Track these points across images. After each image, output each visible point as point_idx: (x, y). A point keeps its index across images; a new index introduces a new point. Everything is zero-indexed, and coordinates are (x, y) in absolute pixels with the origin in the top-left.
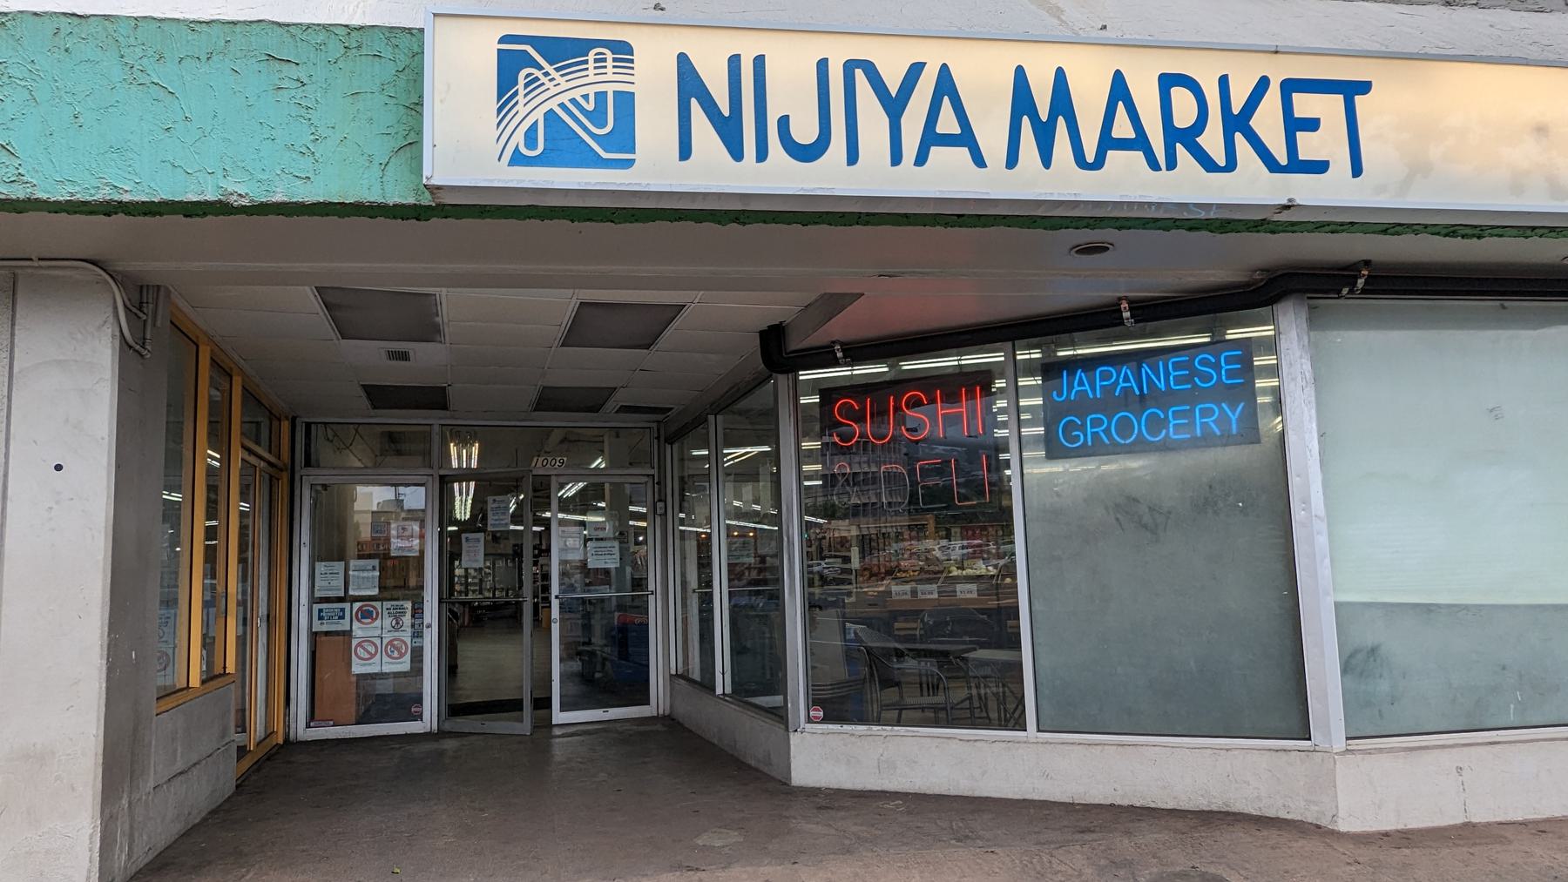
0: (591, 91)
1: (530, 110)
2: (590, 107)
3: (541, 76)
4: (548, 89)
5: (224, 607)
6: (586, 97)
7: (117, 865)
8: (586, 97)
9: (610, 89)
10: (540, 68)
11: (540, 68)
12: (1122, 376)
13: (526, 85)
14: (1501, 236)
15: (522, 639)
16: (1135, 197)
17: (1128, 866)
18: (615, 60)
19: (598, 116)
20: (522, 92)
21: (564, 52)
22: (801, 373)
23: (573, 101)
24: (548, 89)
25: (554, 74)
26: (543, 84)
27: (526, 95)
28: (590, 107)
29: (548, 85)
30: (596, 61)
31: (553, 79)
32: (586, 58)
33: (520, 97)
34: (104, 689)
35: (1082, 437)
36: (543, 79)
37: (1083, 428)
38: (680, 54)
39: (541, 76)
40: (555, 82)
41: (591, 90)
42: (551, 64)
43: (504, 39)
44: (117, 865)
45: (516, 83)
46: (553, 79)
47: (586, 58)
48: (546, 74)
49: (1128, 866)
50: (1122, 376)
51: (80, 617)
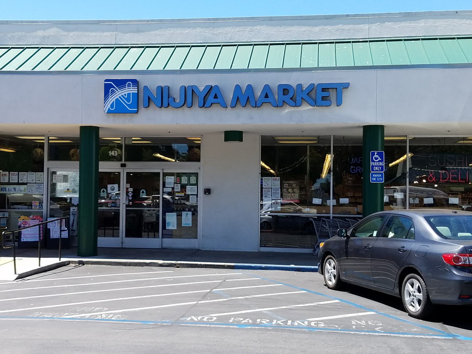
1: (112, 99)
3: (115, 90)
4: (117, 93)
6: (125, 95)
7: (301, 159)
9: (131, 92)
11: (115, 88)
12: (355, 160)
13: (111, 93)
14: (24, 198)
18: (132, 85)
19: (128, 100)
20: (110, 95)
24: (117, 93)
25: (118, 89)
26: (115, 92)
27: (111, 95)
29: (117, 92)
30: (128, 85)
31: (118, 90)
32: (119, 98)
33: (110, 96)
35: (355, 171)
37: (356, 169)
39: (115, 90)
40: (118, 91)
41: (126, 93)
42: (117, 87)
43: (106, 80)
44: (301, 159)
45: (109, 92)
47: (119, 98)
48: (116, 89)
50: (355, 160)
51: (24, 122)
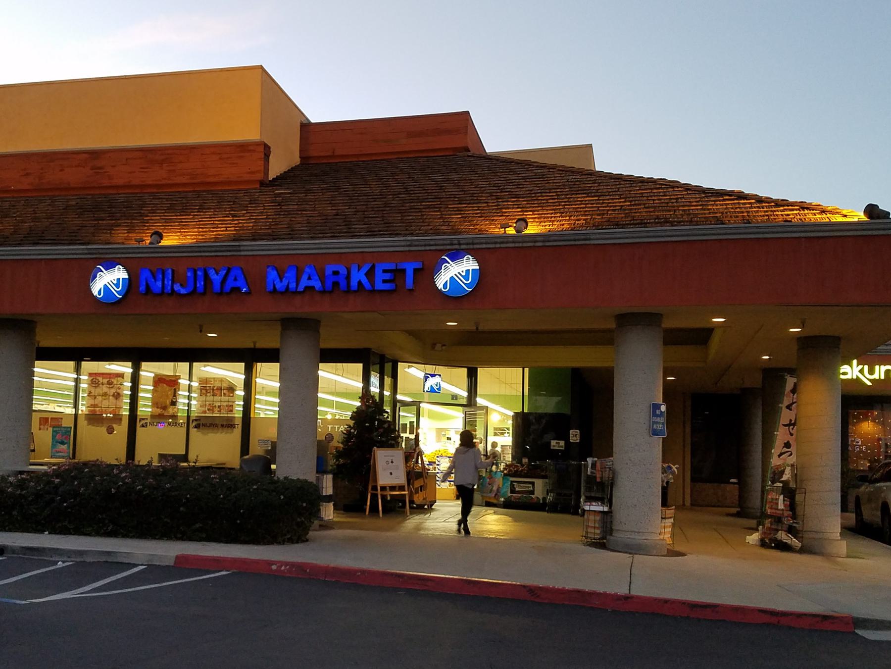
0: (464, 270)
2: (464, 274)
5: (149, 370)
6: (463, 271)
8: (463, 271)
10: (449, 263)
11: (449, 263)
15: (842, 393)
16: (616, 413)
17: (504, 455)
21: (143, 419)
22: (527, 370)
23: (459, 273)
28: (464, 274)
31: (451, 265)
34: (586, 346)
36: (450, 267)
38: (109, 433)
46: (451, 265)
49: (504, 455)
